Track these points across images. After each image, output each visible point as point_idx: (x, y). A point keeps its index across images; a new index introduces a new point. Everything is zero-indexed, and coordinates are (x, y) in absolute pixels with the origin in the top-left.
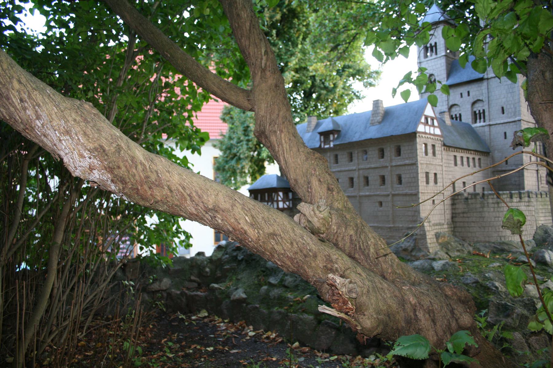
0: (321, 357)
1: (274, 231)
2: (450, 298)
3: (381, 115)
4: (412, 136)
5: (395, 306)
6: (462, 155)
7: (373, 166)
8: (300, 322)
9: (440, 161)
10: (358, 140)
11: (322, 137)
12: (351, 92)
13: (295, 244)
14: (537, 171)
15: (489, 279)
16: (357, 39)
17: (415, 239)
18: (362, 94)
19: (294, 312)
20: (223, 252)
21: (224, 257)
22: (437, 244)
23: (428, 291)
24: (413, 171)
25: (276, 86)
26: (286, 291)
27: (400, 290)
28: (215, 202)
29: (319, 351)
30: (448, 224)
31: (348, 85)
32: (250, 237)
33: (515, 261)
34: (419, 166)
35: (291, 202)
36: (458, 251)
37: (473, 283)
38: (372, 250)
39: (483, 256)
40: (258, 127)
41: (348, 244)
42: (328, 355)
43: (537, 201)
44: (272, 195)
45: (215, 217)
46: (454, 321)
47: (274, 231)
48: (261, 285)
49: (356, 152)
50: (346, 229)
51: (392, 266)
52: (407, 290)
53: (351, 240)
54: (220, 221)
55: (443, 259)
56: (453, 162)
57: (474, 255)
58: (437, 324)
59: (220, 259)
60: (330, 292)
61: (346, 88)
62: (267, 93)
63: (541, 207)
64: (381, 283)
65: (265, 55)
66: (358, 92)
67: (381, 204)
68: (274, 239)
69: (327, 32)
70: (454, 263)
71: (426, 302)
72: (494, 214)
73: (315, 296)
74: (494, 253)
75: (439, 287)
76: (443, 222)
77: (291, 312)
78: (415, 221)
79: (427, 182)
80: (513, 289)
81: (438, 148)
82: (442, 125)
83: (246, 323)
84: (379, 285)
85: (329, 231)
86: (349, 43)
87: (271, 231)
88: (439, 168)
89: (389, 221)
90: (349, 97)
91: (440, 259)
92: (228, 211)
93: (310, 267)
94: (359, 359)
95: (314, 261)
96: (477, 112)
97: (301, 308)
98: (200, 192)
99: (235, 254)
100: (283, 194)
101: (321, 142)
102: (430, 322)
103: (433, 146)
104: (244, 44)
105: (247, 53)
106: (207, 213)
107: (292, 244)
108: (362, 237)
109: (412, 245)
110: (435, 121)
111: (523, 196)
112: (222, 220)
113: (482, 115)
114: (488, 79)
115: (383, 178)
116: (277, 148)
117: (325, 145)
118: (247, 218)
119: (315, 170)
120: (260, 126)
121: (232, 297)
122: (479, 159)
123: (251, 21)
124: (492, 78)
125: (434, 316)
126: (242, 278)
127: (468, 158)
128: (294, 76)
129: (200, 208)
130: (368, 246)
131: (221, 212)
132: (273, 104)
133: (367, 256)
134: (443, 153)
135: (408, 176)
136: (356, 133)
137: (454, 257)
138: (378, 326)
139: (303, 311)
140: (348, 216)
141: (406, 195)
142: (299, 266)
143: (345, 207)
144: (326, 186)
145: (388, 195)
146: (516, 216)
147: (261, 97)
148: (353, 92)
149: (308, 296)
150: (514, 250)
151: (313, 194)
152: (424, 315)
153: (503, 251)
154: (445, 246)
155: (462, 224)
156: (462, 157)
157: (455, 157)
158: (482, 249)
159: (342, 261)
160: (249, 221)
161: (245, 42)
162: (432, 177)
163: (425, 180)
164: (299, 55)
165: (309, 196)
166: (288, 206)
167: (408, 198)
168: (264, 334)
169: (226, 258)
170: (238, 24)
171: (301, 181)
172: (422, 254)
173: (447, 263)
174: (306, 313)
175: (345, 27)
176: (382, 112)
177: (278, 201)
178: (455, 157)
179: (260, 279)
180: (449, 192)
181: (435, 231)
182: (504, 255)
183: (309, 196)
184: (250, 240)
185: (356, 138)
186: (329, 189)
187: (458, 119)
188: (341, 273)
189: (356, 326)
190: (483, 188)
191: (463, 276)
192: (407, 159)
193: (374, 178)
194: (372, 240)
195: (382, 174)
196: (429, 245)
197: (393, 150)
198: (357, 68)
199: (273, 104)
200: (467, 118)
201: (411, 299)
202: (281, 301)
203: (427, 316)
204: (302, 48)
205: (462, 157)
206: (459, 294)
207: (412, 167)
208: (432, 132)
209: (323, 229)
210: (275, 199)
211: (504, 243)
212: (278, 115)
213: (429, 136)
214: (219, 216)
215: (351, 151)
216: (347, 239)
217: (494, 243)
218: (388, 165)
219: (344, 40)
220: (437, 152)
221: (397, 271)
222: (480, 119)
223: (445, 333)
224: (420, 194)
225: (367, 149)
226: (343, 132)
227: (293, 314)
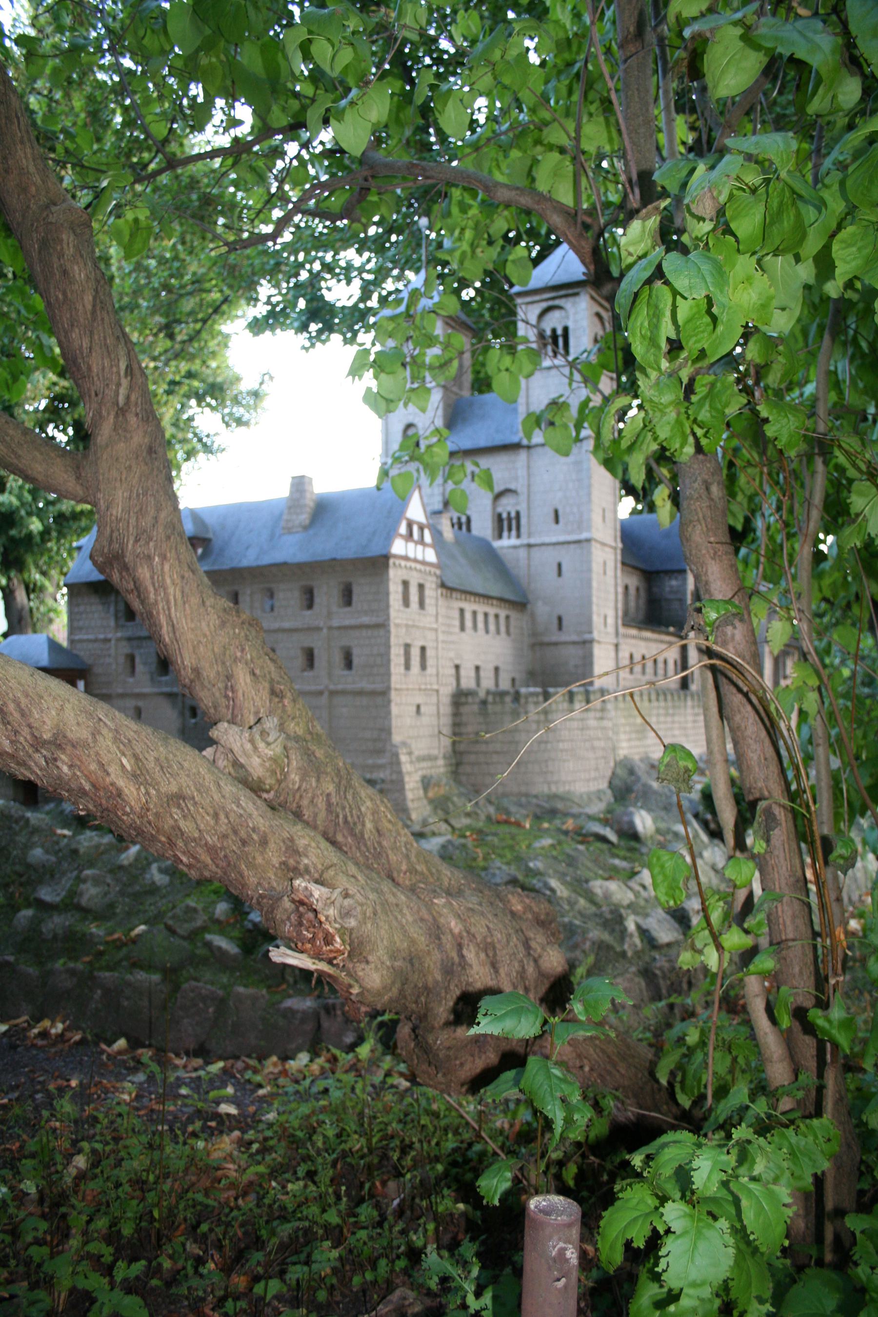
0: (185, 1067)
1: (180, 789)
2: (520, 918)
4: (379, 563)
5: (422, 940)
6: (475, 607)
7: (287, 625)
9: (433, 619)
10: (254, 564)
12: (190, 436)
13: (222, 816)
14: (617, 646)
15: (536, 873)
16: (223, 313)
18: (218, 442)
22: (425, 802)
23: (480, 904)
25: (151, 450)
26: (85, 919)
27: (429, 906)
28: (58, 725)
29: (178, 1055)
30: (445, 757)
31: (185, 416)
32: (127, 803)
33: (580, 835)
34: (393, 629)
36: (468, 815)
38: (369, 825)
39: (518, 824)
40: (105, 543)
41: (322, 815)
42: (199, 1062)
43: (616, 708)
45: (55, 760)
46: (532, 963)
47: (180, 789)
48: (15, 909)
50: (318, 780)
51: (407, 857)
52: (444, 906)
53: (329, 804)
54: (65, 769)
55: (440, 834)
56: (457, 623)
57: (498, 822)
58: (501, 971)
60: (293, 918)
61: (183, 425)
62: (130, 467)
63: (623, 721)
64: (394, 895)
65: (126, 376)
66: (208, 436)
68: (179, 806)
69: (154, 289)
70: (463, 841)
71: (480, 930)
73: (162, 926)
74: (537, 818)
75: (498, 896)
76: (435, 752)
77: (101, 969)
78: (380, 752)
79: (407, 667)
80: (666, 894)
81: (429, 592)
82: (438, 542)
84: (392, 899)
85: (283, 785)
86: (204, 321)
87: (174, 788)
88: (431, 635)
90: (187, 447)
91: (434, 834)
92: (86, 745)
93: (251, 866)
94: (275, 1065)
95: (262, 853)
96: (505, 516)
98: (24, 701)
102: (488, 969)
103: (421, 587)
104: (76, 344)
105: (84, 368)
106: (37, 751)
107: (216, 816)
108: (350, 797)
110: (427, 532)
111: (592, 697)
112: (71, 767)
113: (514, 523)
114: (529, 447)
115: (310, 656)
116: (152, 596)
118: (124, 761)
119: (243, 650)
120: (111, 541)
122: (507, 617)
123: (96, 291)
124: (537, 446)
125: (495, 955)
127: (486, 615)
128: (55, 384)
129: (22, 739)
130: (361, 817)
131: (69, 748)
132: (145, 494)
133: (359, 838)
134: (440, 603)
137: (460, 830)
138: (393, 983)
139: (134, 965)
140: (320, 753)
141: (360, 693)
142: (229, 865)
143: (311, 733)
144: (267, 685)
145: (321, 693)
146: (682, 759)
147: (114, 473)
148: (196, 435)
150: (575, 810)
151: (238, 702)
152: (477, 954)
153: (553, 813)
154: (441, 805)
156: (474, 613)
157: (462, 611)
158: (513, 809)
159: (315, 851)
160: (128, 767)
161: (79, 339)
162: (415, 653)
163: (402, 660)
165: (227, 707)
167: (365, 701)
168: (31, 1027)
170: (64, 294)
171: (210, 672)
173: (449, 842)
174: (142, 968)
175: (197, 281)
176: (312, 504)
178: (462, 611)
179: (12, 893)
180: (447, 690)
181: (420, 773)
182: (557, 822)
183: (227, 707)
184: (128, 809)
185: (249, 559)
186: (273, 692)
187: (464, 527)
188: (316, 875)
189: (350, 986)
190: (513, 680)
191: (485, 869)
194: (369, 803)
195: (306, 644)
196: (410, 805)
197: (336, 594)
198: (210, 380)
199: (145, 494)
200: (483, 527)
201: (453, 924)
202: (74, 944)
203: (482, 956)
205: (474, 613)
206: (536, 909)
208: (420, 557)
209: (269, 781)
211: (555, 796)
212: (156, 518)
213: (413, 565)
214: (63, 757)
215: (236, 588)
216: (321, 803)
217: (536, 796)
218: (321, 624)
219: (192, 313)
220: (428, 601)
221: (418, 868)
222: (510, 529)
223: (515, 987)
226: (217, 544)
227: (107, 974)
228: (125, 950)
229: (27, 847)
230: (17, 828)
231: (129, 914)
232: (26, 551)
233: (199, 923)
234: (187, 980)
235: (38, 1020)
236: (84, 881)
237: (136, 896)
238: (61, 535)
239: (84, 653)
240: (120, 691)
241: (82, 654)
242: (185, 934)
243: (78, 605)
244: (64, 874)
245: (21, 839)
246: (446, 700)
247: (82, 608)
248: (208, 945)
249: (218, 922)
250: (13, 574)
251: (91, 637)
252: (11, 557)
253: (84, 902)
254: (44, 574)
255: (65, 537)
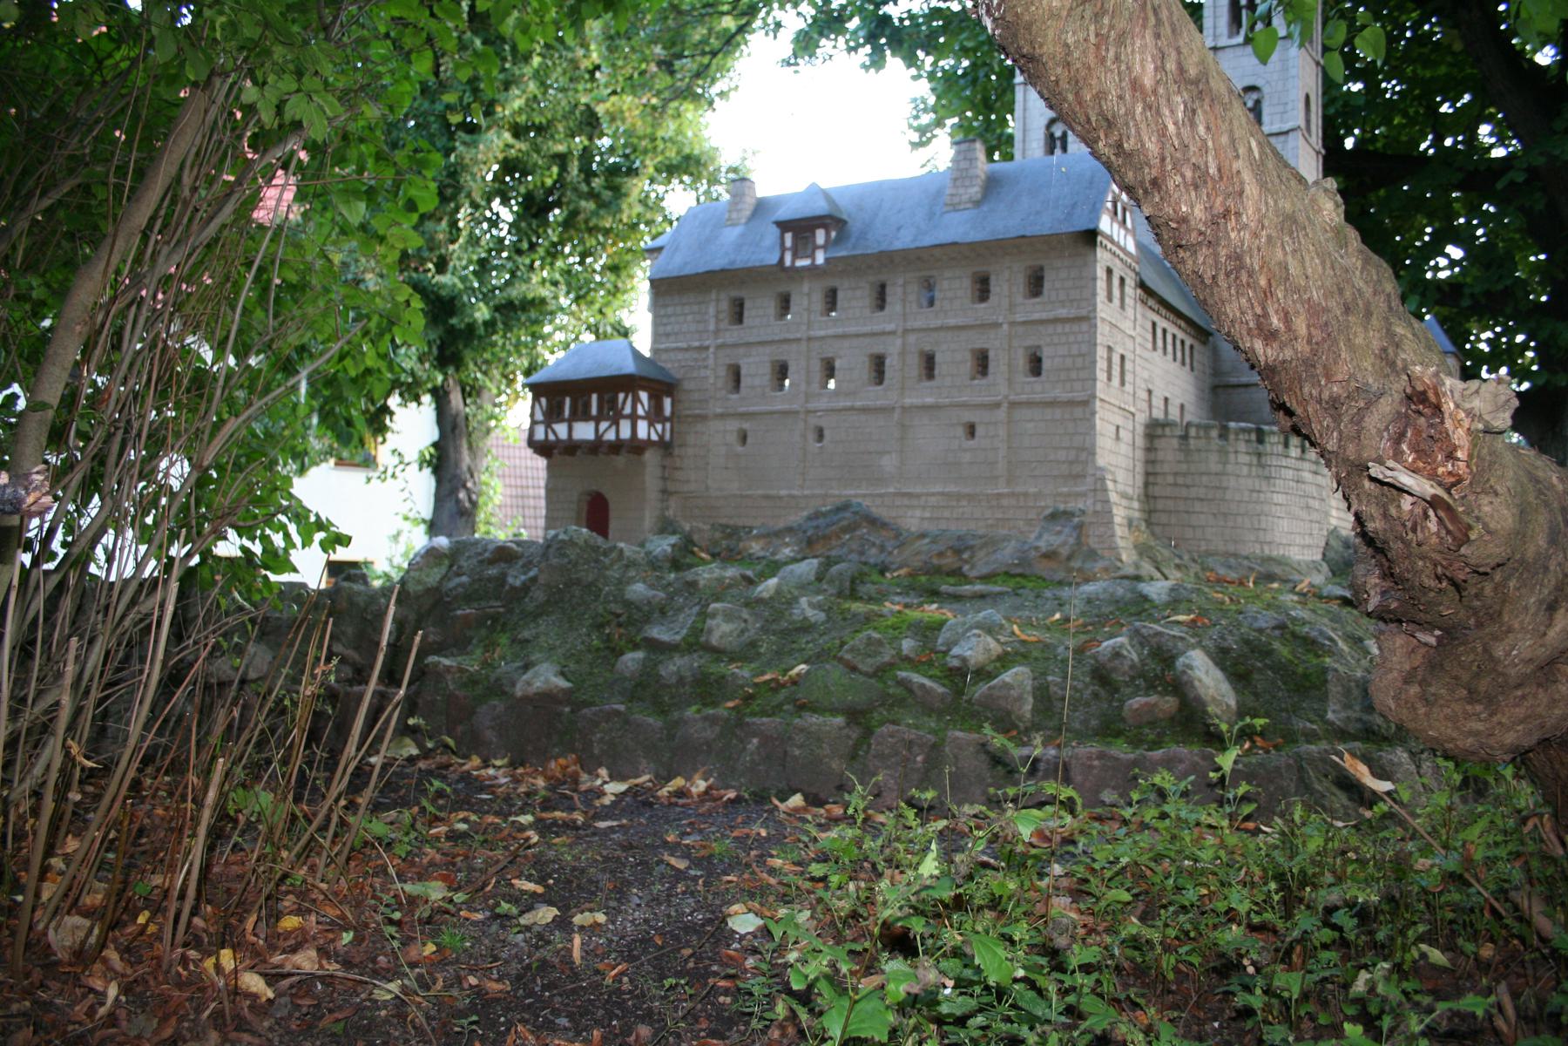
3: (979, 182)
7: (952, 322)
8: (800, 739)
11: (788, 237)
17: (1080, 526)
19: (764, 713)
20: (444, 569)
21: (451, 584)
24: (1080, 338)
35: (668, 425)
37: (1274, 628)
44: (614, 400)
49: (900, 281)
59: (435, 592)
67: (971, 430)
72: (1250, 482)
77: (753, 714)
78: (1080, 477)
83: (579, 761)
89: (997, 478)
97: (788, 700)
99: (492, 571)
100: (650, 398)
101: (783, 250)
109: (1071, 541)
117: (795, 256)
121: (519, 691)
122: (1192, 347)
126: (537, 636)
128: (509, 146)
135: (1062, 350)
136: (899, 229)
141: (1052, 404)
145: (997, 405)
149: (803, 666)
155: (1170, 504)
164: (532, 87)
166: (661, 437)
167: (1058, 413)
169: (461, 585)
172: (1099, 565)
174: (814, 710)
177: (634, 418)
178: (1154, 324)
180: (1142, 418)
185: (904, 240)
192: (1063, 304)
193: (954, 358)
195: (979, 344)
198: (687, 151)
202: (707, 689)
204: (540, 64)
207: (1075, 328)
210: (628, 410)
211: (1270, 559)
215: (883, 277)
217: (1247, 558)
224: (1098, 403)
225: (934, 273)
226: (855, 226)
227: (765, 720)
228: (783, 693)
229: (622, 583)
230: (607, 561)
231: (779, 654)
232: (466, 346)
233: (887, 659)
234: (882, 724)
235: (669, 779)
236: (713, 616)
237: (784, 633)
238: (508, 328)
239: (673, 366)
240: (719, 410)
241: (669, 366)
242: (870, 670)
243: (666, 306)
244: (680, 610)
245: (614, 573)
246: (1140, 430)
247: (670, 310)
248: (904, 684)
249: (907, 659)
250: (451, 371)
251: (684, 345)
252: (448, 353)
253: (714, 640)
254: (485, 373)
255: (511, 331)
